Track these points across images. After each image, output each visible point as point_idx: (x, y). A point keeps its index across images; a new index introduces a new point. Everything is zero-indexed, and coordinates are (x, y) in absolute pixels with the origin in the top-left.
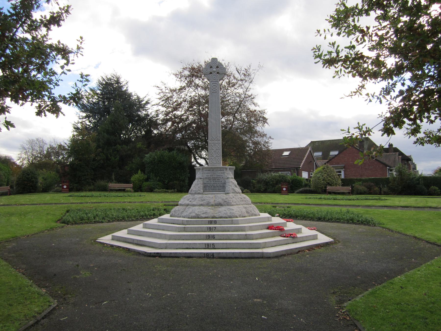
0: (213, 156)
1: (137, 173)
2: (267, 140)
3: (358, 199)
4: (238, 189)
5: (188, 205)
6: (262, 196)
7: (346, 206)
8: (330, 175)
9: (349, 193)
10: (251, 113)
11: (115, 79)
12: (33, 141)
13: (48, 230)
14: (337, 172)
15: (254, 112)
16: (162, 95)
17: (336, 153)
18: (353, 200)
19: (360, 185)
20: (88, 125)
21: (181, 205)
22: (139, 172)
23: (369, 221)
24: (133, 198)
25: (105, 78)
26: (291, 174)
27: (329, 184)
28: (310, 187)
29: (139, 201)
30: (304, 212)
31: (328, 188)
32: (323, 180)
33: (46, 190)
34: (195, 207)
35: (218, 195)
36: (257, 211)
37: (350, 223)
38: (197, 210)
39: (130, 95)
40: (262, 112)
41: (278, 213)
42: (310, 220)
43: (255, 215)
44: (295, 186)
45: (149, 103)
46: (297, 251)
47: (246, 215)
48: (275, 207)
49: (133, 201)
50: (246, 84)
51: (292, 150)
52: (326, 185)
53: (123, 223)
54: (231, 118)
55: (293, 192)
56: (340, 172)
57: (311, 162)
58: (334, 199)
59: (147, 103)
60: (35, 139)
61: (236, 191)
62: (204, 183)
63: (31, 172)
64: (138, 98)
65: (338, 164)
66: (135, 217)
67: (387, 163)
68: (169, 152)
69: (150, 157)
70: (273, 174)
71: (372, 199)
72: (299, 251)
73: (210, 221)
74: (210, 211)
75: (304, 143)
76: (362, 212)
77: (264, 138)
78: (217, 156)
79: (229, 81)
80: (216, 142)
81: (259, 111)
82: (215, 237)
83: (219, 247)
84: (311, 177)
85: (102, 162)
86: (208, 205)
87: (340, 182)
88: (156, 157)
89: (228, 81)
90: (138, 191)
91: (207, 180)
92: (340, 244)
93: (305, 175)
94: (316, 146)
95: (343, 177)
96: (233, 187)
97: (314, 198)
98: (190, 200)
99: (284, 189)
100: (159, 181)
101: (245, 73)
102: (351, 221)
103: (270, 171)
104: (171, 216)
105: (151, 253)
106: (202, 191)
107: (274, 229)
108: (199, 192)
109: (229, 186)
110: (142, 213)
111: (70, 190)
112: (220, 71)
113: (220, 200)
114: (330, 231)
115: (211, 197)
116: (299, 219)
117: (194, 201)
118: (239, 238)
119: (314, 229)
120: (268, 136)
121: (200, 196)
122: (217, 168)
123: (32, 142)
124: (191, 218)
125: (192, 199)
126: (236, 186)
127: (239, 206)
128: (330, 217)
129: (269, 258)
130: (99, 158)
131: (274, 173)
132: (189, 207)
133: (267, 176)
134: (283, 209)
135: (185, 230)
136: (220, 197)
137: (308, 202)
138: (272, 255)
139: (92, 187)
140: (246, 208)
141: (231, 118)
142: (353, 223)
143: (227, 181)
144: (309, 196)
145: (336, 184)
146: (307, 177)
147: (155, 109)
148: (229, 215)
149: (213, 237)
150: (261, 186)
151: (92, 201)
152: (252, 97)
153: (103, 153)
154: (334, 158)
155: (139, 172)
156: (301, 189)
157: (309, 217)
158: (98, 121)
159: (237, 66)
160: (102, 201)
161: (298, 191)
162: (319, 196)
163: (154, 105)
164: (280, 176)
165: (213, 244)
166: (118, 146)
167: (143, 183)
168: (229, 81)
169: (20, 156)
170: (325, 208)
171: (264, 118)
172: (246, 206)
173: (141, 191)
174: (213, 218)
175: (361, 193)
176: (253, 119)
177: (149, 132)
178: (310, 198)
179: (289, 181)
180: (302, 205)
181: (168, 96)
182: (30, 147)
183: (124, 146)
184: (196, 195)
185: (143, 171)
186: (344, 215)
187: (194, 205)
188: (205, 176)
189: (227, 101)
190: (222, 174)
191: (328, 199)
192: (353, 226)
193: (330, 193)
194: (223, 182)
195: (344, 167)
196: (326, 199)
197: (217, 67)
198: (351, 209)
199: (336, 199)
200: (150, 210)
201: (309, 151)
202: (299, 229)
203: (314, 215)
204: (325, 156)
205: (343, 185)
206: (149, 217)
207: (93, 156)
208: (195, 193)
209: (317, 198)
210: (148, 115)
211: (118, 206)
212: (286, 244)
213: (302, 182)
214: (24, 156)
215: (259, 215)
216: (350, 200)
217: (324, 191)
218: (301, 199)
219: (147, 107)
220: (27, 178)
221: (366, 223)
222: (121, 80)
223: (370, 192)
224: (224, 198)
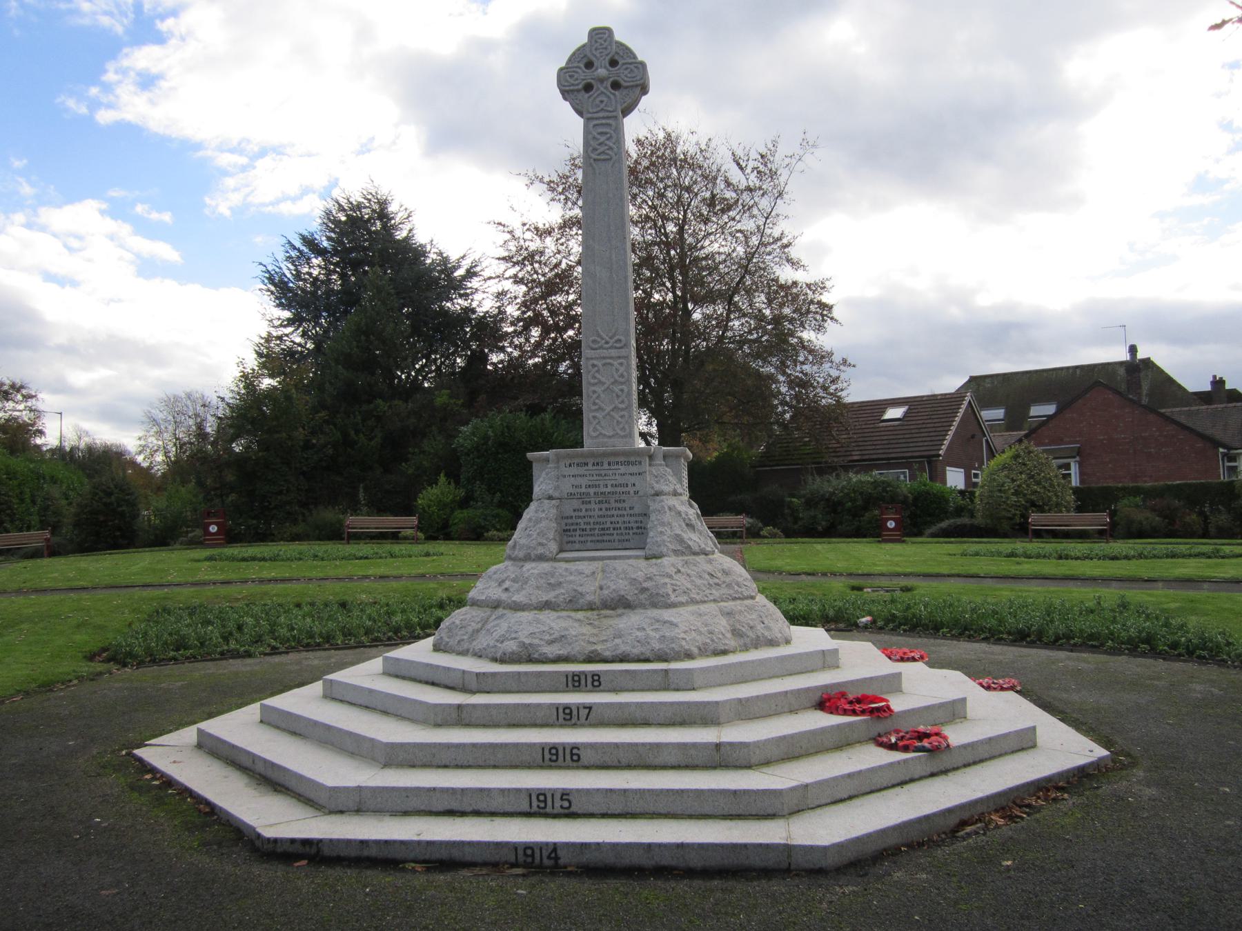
0: (600, 409)
1: (433, 482)
2: (834, 373)
3: (1141, 556)
4: (701, 537)
5: (496, 605)
6: (819, 547)
7: (1106, 580)
8: (1037, 478)
9: (1101, 533)
10: (784, 293)
11: (376, 207)
12: (177, 399)
13: (27, 693)
14: (1060, 467)
15: (789, 288)
16: (512, 246)
17: (1050, 409)
18: (1127, 557)
19: (1137, 506)
20: (300, 345)
21: (475, 603)
22: (442, 478)
23: (1218, 646)
24: (397, 562)
25: (343, 202)
26: (913, 477)
27: (1033, 504)
28: (972, 516)
29: (414, 572)
30: (964, 611)
31: (1034, 517)
32: (1016, 493)
33: (163, 538)
34: (520, 614)
35: (620, 565)
36: (777, 621)
37: (1144, 655)
38: (525, 627)
39: (420, 252)
40: (819, 287)
41: (870, 613)
42: (986, 639)
43: (772, 643)
44: (925, 515)
45: (475, 274)
46: (953, 821)
47: (732, 642)
48: (860, 589)
49: (395, 573)
50: (764, 203)
51: (913, 404)
52: (1026, 509)
53: (314, 659)
54: (720, 309)
55: (919, 534)
56: (1067, 467)
57: (973, 437)
58: (1060, 558)
59: (471, 274)
60: (183, 395)
61: (689, 547)
62: (562, 517)
63: (116, 487)
64: (445, 260)
65: (1061, 441)
66: (368, 632)
67: (1218, 434)
68: (531, 417)
69: (473, 434)
70: (854, 478)
71: (1190, 556)
72: (964, 823)
73: (574, 674)
74: (577, 629)
75: (950, 384)
76: (1173, 605)
77: (826, 366)
78: (615, 409)
79: (713, 196)
80: (614, 353)
81: (809, 286)
82: (582, 753)
83: (592, 809)
84: (975, 485)
85: (331, 451)
86: (573, 604)
87: (1071, 498)
88: (490, 433)
89: (708, 195)
90: (435, 538)
91: (576, 504)
92: (1140, 773)
93: (955, 478)
94: (985, 388)
95: (1075, 481)
96: (679, 529)
97: (992, 554)
98: (507, 584)
99: (891, 524)
100: (501, 505)
101: (762, 168)
102: (1144, 645)
103: (846, 468)
104: (437, 648)
105: (276, 841)
106: (553, 547)
107: (845, 712)
108: (540, 550)
109: (663, 524)
110: (398, 618)
111: (231, 537)
112: (622, 75)
113: (622, 587)
114: (1075, 697)
115: (588, 573)
116: (944, 637)
117: (518, 591)
118: (688, 760)
119: (1012, 688)
120: (837, 358)
121: (546, 566)
122: (615, 454)
123: (174, 405)
124: (502, 661)
125: (514, 581)
126: (690, 526)
127: (703, 607)
128: (1062, 629)
129: (817, 872)
130: (322, 441)
131: (857, 473)
132: (500, 611)
133: (835, 482)
134: (888, 596)
135: (460, 717)
136: (625, 570)
137: (974, 570)
138: (830, 861)
139: (300, 528)
140: (729, 614)
141: (720, 309)
142: (1155, 653)
143: (653, 506)
144: (972, 545)
145: (1058, 505)
146: (961, 486)
147: (491, 293)
148: (657, 646)
149: (570, 757)
150: (815, 517)
151: (265, 574)
152: (785, 241)
153: (335, 425)
154: (1043, 424)
155: (442, 478)
156: (944, 524)
157: (982, 630)
158: (326, 331)
159: (735, 147)
160: (295, 575)
161: (934, 529)
162: (1006, 546)
163: (490, 278)
164: (875, 484)
165: (565, 794)
166: (379, 401)
167: (453, 511)
168: (713, 196)
169: (142, 442)
170: (1035, 593)
171: (822, 306)
172: (730, 605)
173: (448, 537)
174: (589, 660)
175: (1141, 534)
176: (787, 311)
177: (478, 359)
178: (977, 554)
179: (906, 497)
180: (952, 580)
181: (531, 249)
182: (170, 418)
183: (396, 402)
184: (528, 566)
185: (454, 476)
186: (1114, 621)
187: (517, 607)
188: (567, 486)
189: (706, 258)
190: (632, 479)
191: (1038, 556)
192: (1160, 665)
193: (1038, 534)
194: (636, 510)
195: (1079, 452)
196: (1030, 557)
197: (613, 63)
198: (1136, 595)
199: (1067, 557)
200: (431, 607)
201: (965, 403)
202: (954, 702)
203: (1001, 622)
204: (1016, 418)
205: (1079, 509)
206: (418, 631)
207: (300, 434)
208: (527, 558)
209: (999, 554)
210: (473, 311)
211: (332, 592)
212: (902, 784)
213: (947, 501)
214: (154, 441)
215: (788, 642)
216: (1114, 558)
217: (1021, 530)
218: (947, 558)
219: (469, 285)
220: (105, 504)
221: (1203, 651)
222: (392, 208)
223: (1170, 529)
224: (640, 575)
